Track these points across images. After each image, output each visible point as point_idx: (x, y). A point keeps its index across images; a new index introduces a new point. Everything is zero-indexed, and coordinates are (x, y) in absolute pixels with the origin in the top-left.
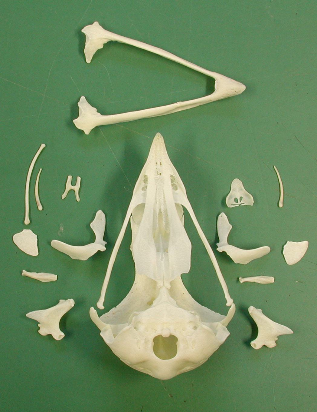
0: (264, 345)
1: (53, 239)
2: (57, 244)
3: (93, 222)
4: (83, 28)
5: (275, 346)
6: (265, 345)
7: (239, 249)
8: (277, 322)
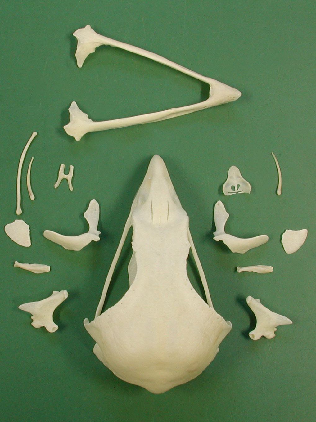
0: (263, 336)
1: (46, 229)
2: (49, 234)
3: (87, 211)
4: (74, 32)
5: (274, 337)
6: (264, 335)
7: (237, 238)
8: (276, 313)
